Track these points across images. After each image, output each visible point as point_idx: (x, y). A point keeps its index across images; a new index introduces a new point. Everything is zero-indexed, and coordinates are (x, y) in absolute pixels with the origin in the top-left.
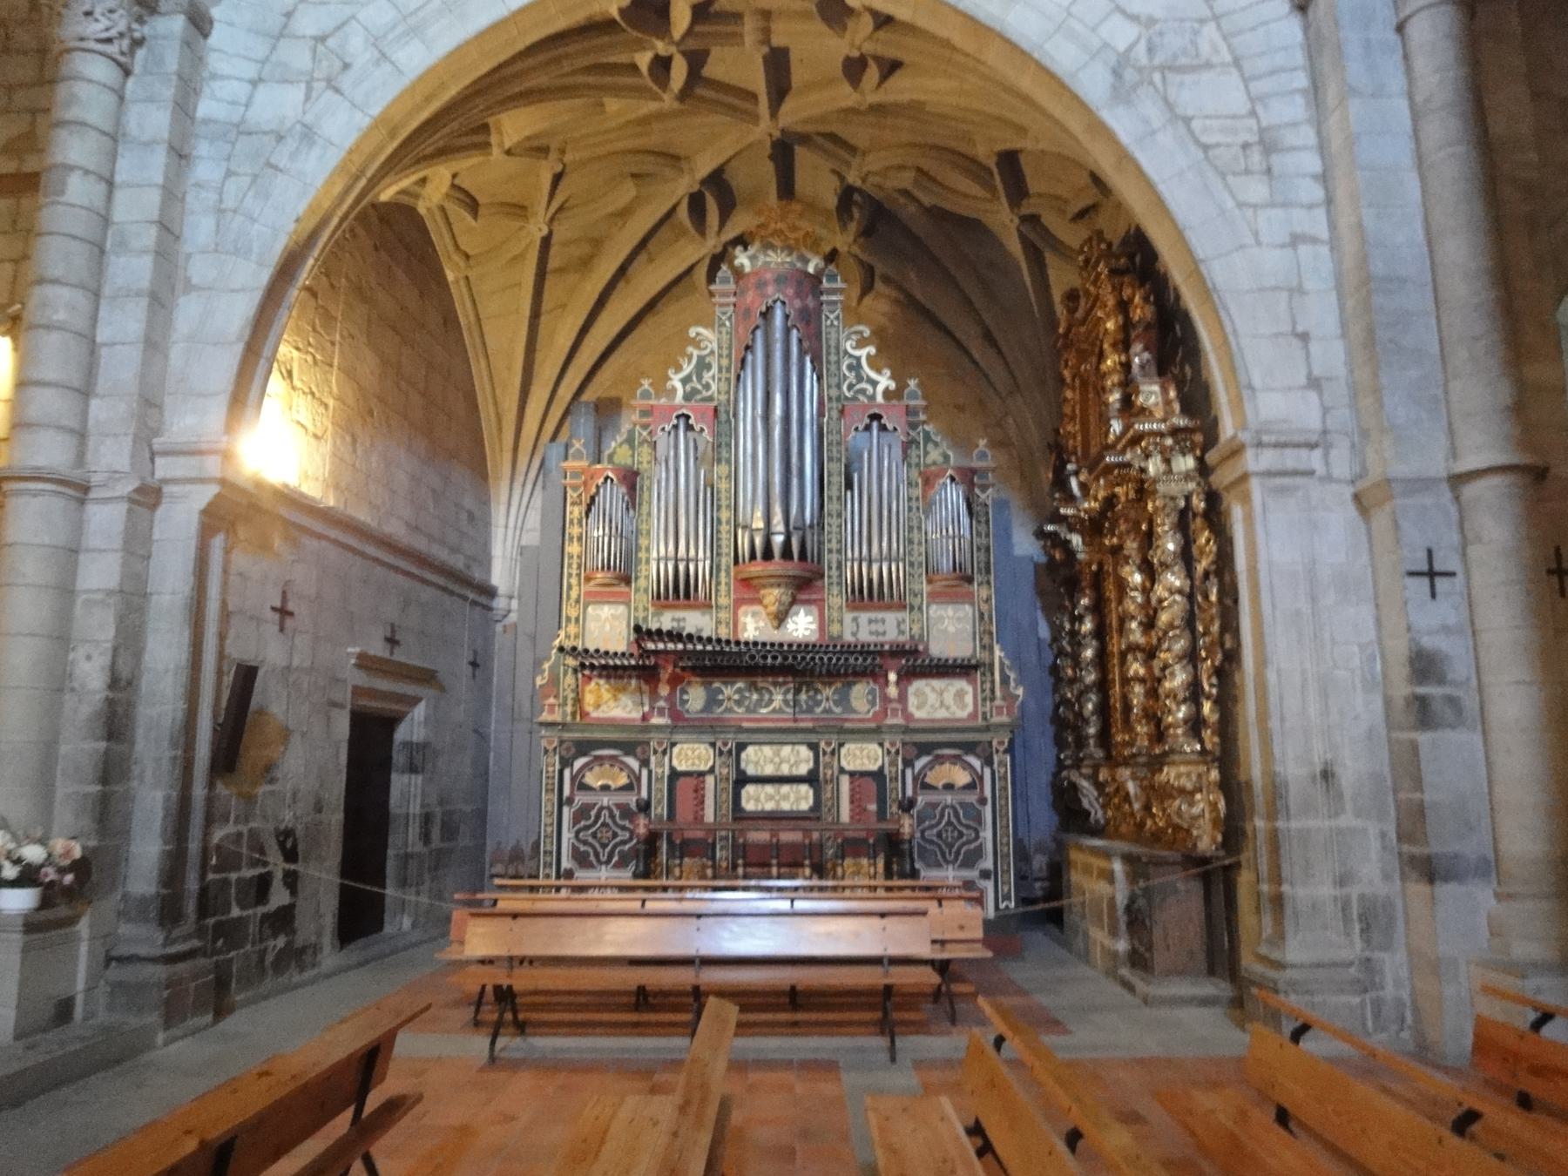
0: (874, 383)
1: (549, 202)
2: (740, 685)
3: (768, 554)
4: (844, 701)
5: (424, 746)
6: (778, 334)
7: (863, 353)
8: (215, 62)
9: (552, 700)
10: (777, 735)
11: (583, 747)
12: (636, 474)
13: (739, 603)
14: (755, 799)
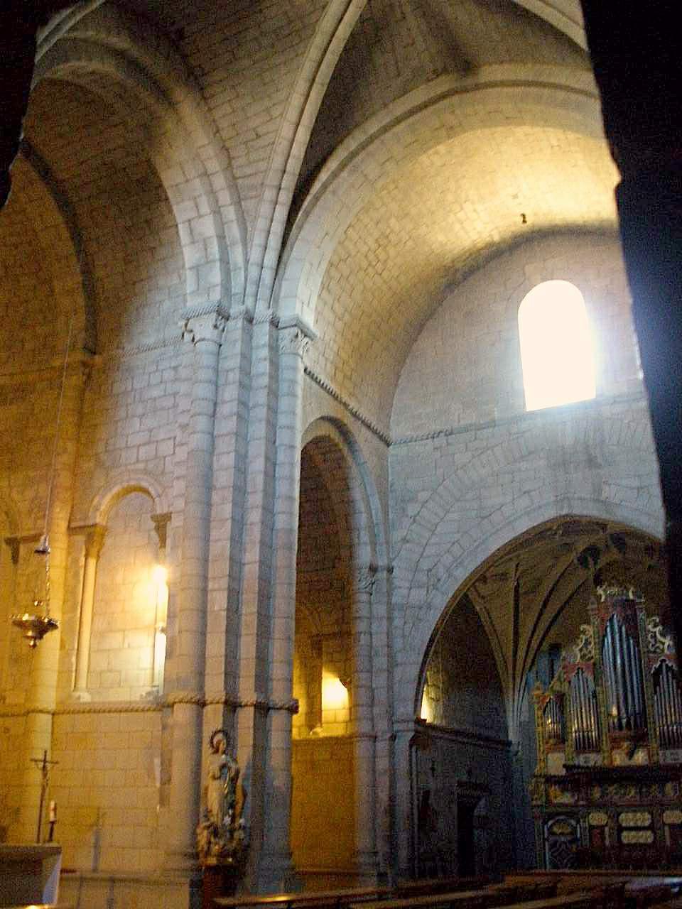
0: (663, 644)
1: (517, 570)
2: (615, 786)
3: (620, 727)
4: (662, 791)
5: (486, 817)
6: (616, 627)
7: (657, 629)
8: (397, 582)
9: (536, 796)
10: (633, 807)
11: (551, 816)
12: (564, 695)
13: (612, 748)
14: (627, 837)
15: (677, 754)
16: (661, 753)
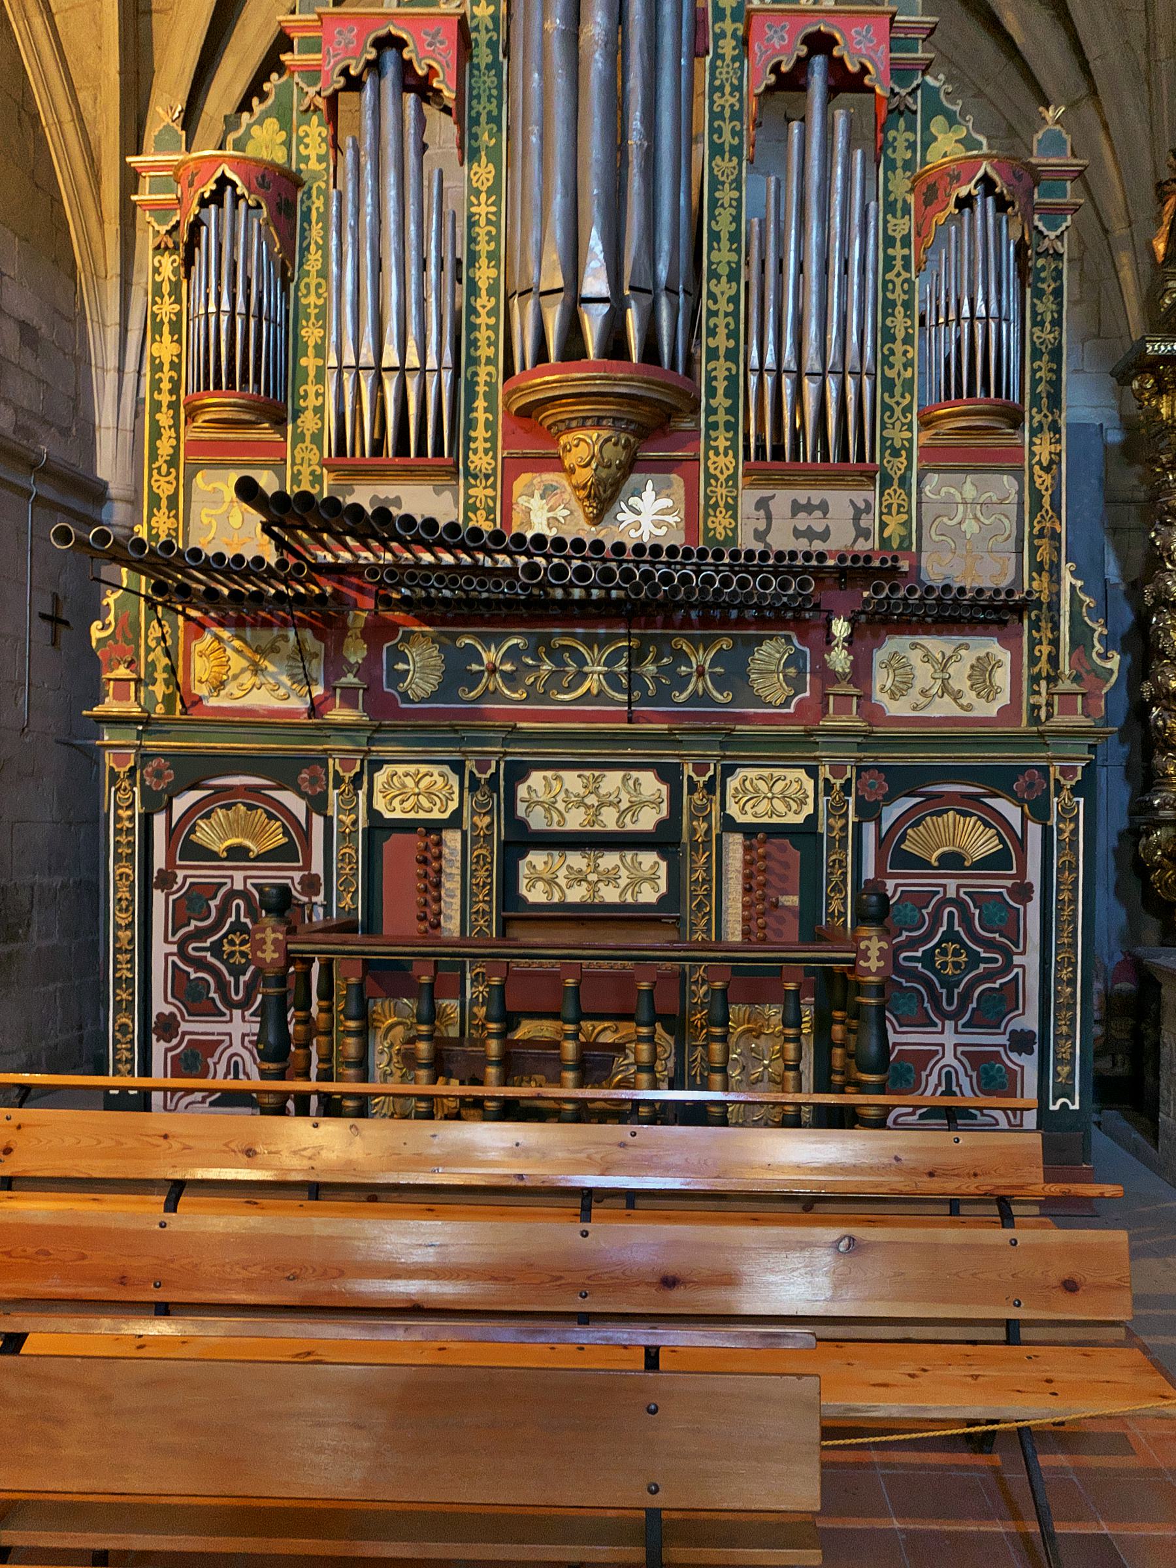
13: (514, 467)
15: (824, 507)
16: (748, 498)
